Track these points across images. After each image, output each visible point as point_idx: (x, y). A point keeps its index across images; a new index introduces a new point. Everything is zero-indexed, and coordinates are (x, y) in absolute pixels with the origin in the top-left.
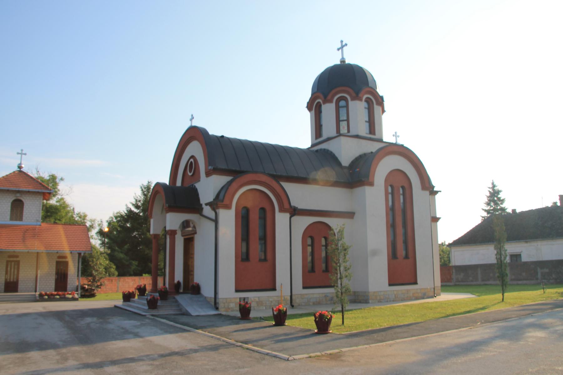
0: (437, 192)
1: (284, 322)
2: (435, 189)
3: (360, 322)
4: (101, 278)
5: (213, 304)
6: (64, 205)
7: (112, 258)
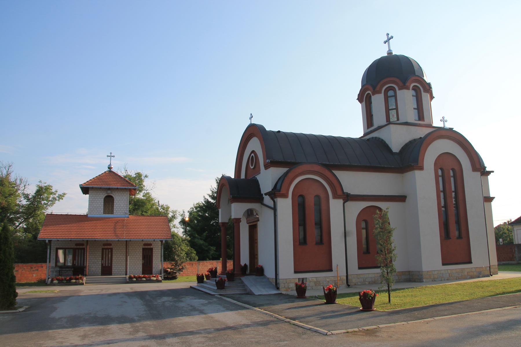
0: (489, 173)
1: (334, 300)
2: (488, 169)
3: (408, 300)
4: (182, 262)
5: (274, 284)
6: (149, 199)
7: (192, 244)
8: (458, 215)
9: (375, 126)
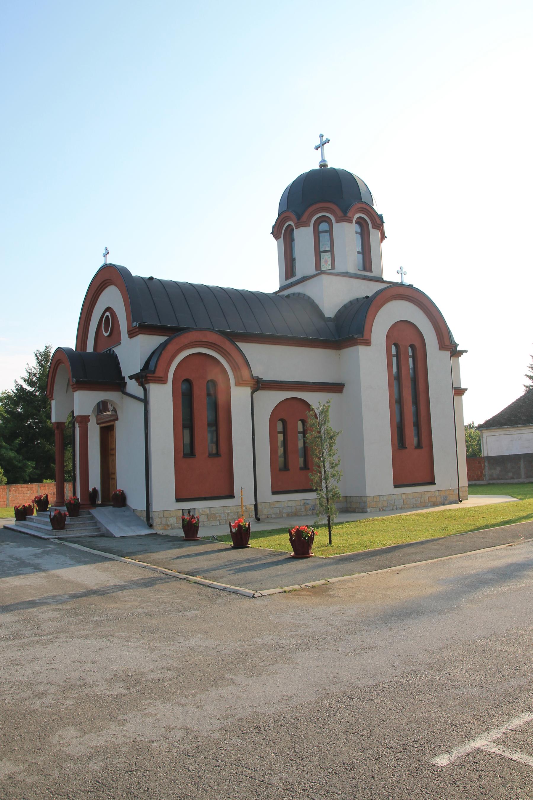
0: (461, 353)
3: (354, 539)
5: (145, 519)
8: (417, 414)
9: (299, 274)
